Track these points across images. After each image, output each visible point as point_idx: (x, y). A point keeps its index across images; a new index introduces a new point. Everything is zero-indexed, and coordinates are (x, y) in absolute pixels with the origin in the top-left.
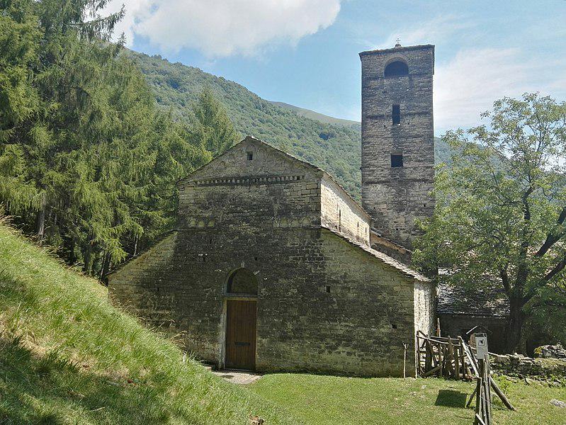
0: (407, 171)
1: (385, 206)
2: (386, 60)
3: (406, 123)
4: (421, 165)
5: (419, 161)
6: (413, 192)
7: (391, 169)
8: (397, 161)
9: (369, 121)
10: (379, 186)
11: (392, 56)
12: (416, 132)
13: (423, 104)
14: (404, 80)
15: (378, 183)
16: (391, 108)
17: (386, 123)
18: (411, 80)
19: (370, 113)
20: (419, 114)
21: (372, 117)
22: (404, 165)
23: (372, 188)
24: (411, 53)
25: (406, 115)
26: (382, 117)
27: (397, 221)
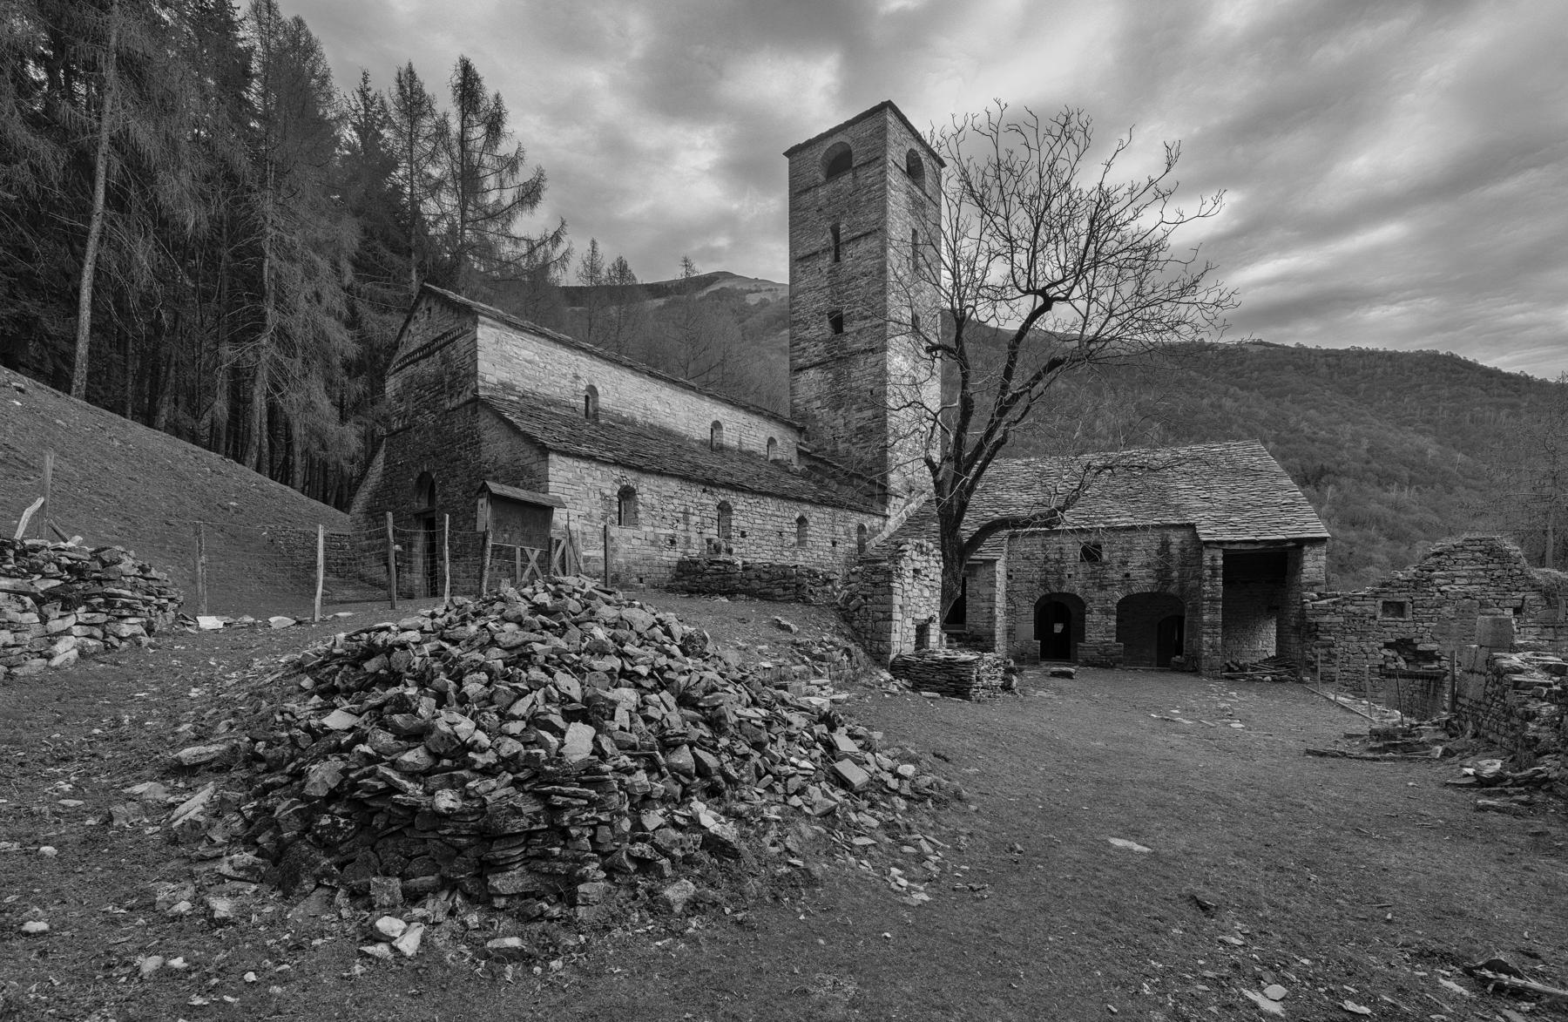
0: (849, 340)
1: (819, 403)
2: (819, 153)
3: (851, 253)
4: (868, 323)
5: (866, 318)
6: (856, 374)
7: (828, 341)
8: (838, 323)
9: (799, 268)
10: (812, 372)
11: (830, 143)
12: (860, 269)
13: (873, 217)
14: (846, 180)
15: (811, 367)
16: (829, 236)
17: (820, 264)
18: (855, 177)
19: (800, 253)
20: (866, 235)
21: (802, 259)
22: (845, 329)
23: (802, 377)
24: (857, 127)
25: (848, 242)
26: (816, 253)
27: (834, 424)
